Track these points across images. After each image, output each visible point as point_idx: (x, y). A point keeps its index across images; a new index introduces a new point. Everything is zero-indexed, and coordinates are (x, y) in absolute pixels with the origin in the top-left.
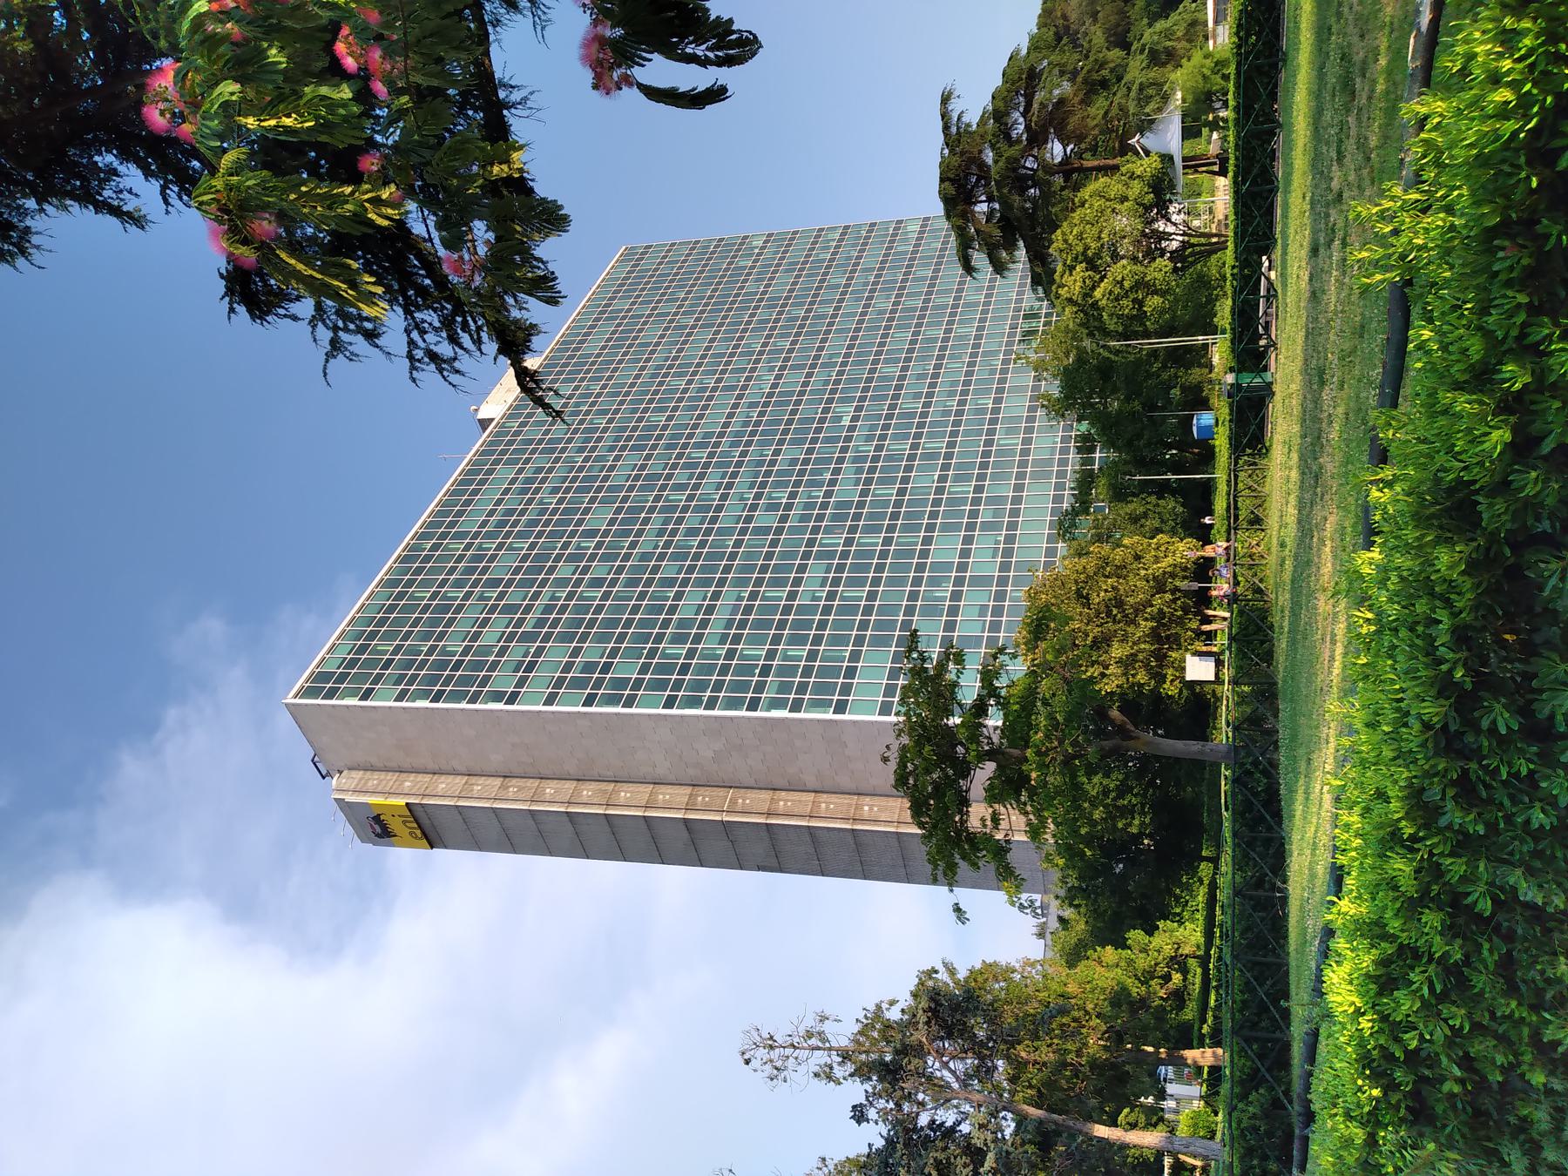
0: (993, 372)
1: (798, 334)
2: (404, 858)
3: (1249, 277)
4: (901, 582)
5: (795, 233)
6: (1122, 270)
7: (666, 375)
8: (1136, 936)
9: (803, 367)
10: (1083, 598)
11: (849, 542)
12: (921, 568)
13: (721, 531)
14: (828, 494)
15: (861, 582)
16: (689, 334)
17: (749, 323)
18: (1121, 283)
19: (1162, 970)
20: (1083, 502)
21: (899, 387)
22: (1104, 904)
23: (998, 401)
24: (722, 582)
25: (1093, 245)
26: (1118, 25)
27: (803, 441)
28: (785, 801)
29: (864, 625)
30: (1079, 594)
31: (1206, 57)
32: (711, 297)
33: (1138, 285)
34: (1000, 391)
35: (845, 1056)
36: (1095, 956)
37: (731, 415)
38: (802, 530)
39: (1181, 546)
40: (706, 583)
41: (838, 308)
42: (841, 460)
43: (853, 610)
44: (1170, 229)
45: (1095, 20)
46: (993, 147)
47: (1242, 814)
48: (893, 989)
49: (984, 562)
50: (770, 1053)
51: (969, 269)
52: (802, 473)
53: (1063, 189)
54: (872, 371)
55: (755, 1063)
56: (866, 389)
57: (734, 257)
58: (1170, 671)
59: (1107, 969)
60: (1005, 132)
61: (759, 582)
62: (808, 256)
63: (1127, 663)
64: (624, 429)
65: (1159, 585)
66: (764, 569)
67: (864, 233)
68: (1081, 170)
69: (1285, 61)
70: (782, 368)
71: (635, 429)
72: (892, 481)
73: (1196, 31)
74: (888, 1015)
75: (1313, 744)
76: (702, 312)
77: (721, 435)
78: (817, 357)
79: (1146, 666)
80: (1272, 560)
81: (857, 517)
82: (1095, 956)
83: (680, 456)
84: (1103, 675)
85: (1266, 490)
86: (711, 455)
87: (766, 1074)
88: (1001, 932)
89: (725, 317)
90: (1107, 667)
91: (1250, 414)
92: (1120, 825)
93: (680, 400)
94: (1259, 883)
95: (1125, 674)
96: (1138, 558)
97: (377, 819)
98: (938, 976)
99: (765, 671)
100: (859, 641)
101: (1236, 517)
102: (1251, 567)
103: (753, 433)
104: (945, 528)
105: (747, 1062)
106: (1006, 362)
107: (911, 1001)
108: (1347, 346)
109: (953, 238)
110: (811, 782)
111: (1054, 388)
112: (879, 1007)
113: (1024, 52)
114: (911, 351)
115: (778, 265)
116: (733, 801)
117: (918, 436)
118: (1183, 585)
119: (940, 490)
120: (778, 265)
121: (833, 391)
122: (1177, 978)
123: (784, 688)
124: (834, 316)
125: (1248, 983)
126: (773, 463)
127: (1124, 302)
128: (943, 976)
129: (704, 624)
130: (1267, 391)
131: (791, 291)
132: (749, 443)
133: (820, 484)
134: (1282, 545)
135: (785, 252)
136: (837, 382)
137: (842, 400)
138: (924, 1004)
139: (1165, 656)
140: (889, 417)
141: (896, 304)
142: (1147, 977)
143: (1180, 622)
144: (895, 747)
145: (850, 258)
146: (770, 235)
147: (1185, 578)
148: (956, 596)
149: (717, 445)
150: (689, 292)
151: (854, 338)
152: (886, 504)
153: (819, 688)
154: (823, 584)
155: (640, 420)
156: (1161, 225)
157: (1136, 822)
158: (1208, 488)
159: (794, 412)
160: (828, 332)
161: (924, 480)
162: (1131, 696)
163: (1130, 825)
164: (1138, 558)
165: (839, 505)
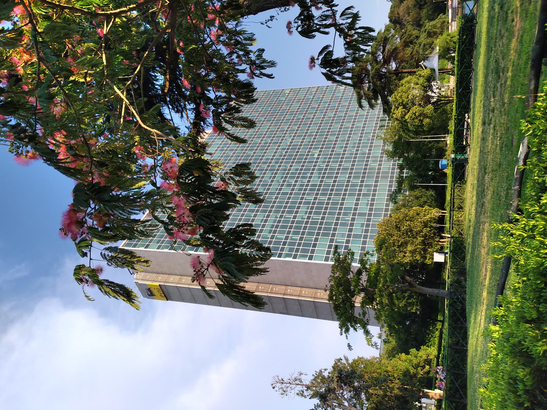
0: (369, 140)
1: (300, 124)
2: (160, 304)
3: (460, 122)
4: (334, 214)
5: (301, 88)
6: (415, 109)
7: (254, 138)
8: (413, 351)
9: (301, 136)
10: (398, 228)
11: (315, 199)
12: (341, 209)
13: (271, 193)
14: (309, 181)
15: (319, 213)
16: (262, 124)
17: (283, 120)
18: (415, 114)
19: (422, 364)
20: (399, 190)
21: (335, 144)
22: (402, 336)
23: (370, 150)
24: (270, 211)
25: (405, 100)
26: (417, 18)
27: (301, 162)
28: (290, 290)
29: (320, 229)
30: (397, 227)
31: (448, 35)
32: (270, 111)
33: (420, 115)
34: (371, 146)
35: (308, 388)
36: (398, 357)
37: (276, 152)
38: (299, 194)
39: (434, 211)
40: (265, 211)
41: (314, 116)
42: (313, 170)
43: (316, 223)
44: (433, 95)
45: (409, 15)
46: (371, 64)
47: (452, 317)
48: (326, 365)
49: (363, 208)
50: (282, 385)
51: (361, 106)
52: (300, 173)
53: (395, 80)
54: (326, 138)
55: (276, 388)
56: (323, 145)
57: (279, 97)
58: (428, 256)
59: (402, 362)
60: (375, 60)
61: (283, 212)
62: (305, 97)
63: (413, 252)
64: (239, 156)
65: (425, 225)
66: (285, 207)
67: (324, 89)
68: (402, 72)
69: (476, 47)
70: (294, 136)
71: (242, 156)
72: (332, 177)
73: (445, 26)
74: (324, 374)
75: (478, 303)
76: (267, 116)
77: (272, 159)
78: (306, 133)
79: (420, 253)
80: (466, 223)
81: (319, 190)
82: (398, 357)
83: (257, 166)
84: (404, 256)
85: (465, 196)
86: (268, 166)
87: (280, 392)
88: (365, 345)
89: (275, 118)
90: (406, 253)
91: (460, 168)
92: (409, 309)
93: (258, 147)
94: (457, 343)
95: (412, 256)
96: (418, 214)
97: (149, 289)
98: (342, 361)
99: (285, 244)
100: (318, 234)
101: (454, 207)
102: (458, 225)
103: (283, 159)
104: (350, 195)
105: (274, 388)
106: (373, 136)
107: (332, 369)
108: (495, 168)
109: (355, 94)
110: (299, 283)
111: (390, 148)
112: (321, 371)
113: (383, 31)
114: (340, 131)
115: (294, 100)
116: (272, 289)
117: (341, 162)
118: (434, 225)
119: (348, 181)
120: (294, 100)
121: (312, 145)
122: (427, 367)
123: (291, 250)
124: (313, 118)
125: (452, 380)
126: (290, 170)
127: (416, 120)
128: (344, 361)
129: (264, 226)
130: (466, 160)
131: (298, 109)
132: (281, 163)
133: (306, 178)
134: (470, 221)
135: (297, 95)
136: (313, 142)
137: (315, 148)
138: (336, 375)
139: (427, 250)
140: (331, 155)
141: (335, 114)
142: (416, 366)
143: (433, 238)
144: (329, 286)
145: (319, 98)
146: (292, 89)
147: (435, 222)
148: (353, 219)
149: (270, 163)
150: (263, 109)
151: (320, 126)
152: (329, 186)
153: (303, 251)
154: (306, 214)
155: (244, 153)
156: (430, 93)
157: (415, 308)
158: (444, 188)
159: (298, 152)
160: (311, 124)
161: (343, 178)
162: (414, 264)
163: (412, 309)
164: (418, 214)
165: (312, 185)
